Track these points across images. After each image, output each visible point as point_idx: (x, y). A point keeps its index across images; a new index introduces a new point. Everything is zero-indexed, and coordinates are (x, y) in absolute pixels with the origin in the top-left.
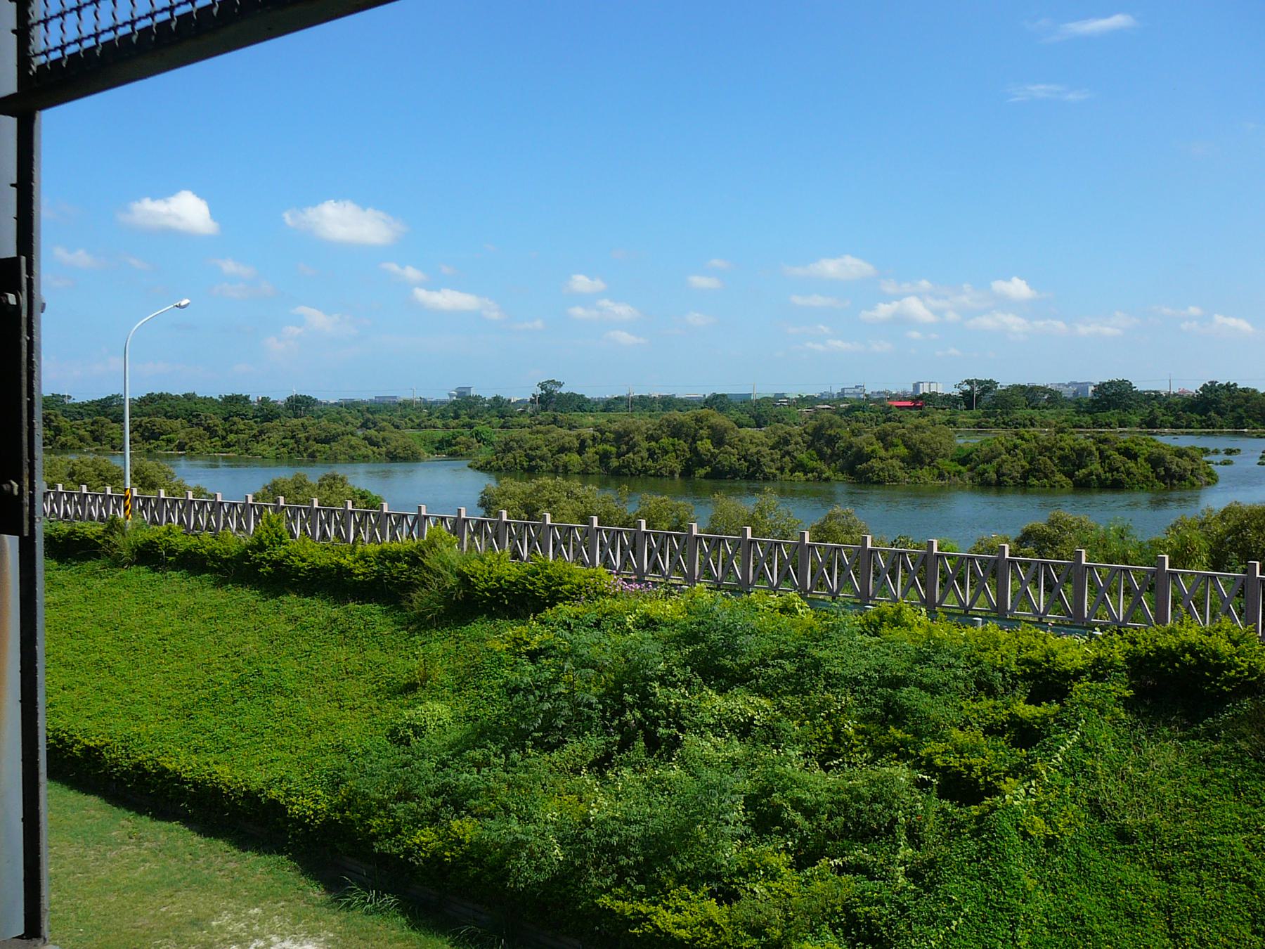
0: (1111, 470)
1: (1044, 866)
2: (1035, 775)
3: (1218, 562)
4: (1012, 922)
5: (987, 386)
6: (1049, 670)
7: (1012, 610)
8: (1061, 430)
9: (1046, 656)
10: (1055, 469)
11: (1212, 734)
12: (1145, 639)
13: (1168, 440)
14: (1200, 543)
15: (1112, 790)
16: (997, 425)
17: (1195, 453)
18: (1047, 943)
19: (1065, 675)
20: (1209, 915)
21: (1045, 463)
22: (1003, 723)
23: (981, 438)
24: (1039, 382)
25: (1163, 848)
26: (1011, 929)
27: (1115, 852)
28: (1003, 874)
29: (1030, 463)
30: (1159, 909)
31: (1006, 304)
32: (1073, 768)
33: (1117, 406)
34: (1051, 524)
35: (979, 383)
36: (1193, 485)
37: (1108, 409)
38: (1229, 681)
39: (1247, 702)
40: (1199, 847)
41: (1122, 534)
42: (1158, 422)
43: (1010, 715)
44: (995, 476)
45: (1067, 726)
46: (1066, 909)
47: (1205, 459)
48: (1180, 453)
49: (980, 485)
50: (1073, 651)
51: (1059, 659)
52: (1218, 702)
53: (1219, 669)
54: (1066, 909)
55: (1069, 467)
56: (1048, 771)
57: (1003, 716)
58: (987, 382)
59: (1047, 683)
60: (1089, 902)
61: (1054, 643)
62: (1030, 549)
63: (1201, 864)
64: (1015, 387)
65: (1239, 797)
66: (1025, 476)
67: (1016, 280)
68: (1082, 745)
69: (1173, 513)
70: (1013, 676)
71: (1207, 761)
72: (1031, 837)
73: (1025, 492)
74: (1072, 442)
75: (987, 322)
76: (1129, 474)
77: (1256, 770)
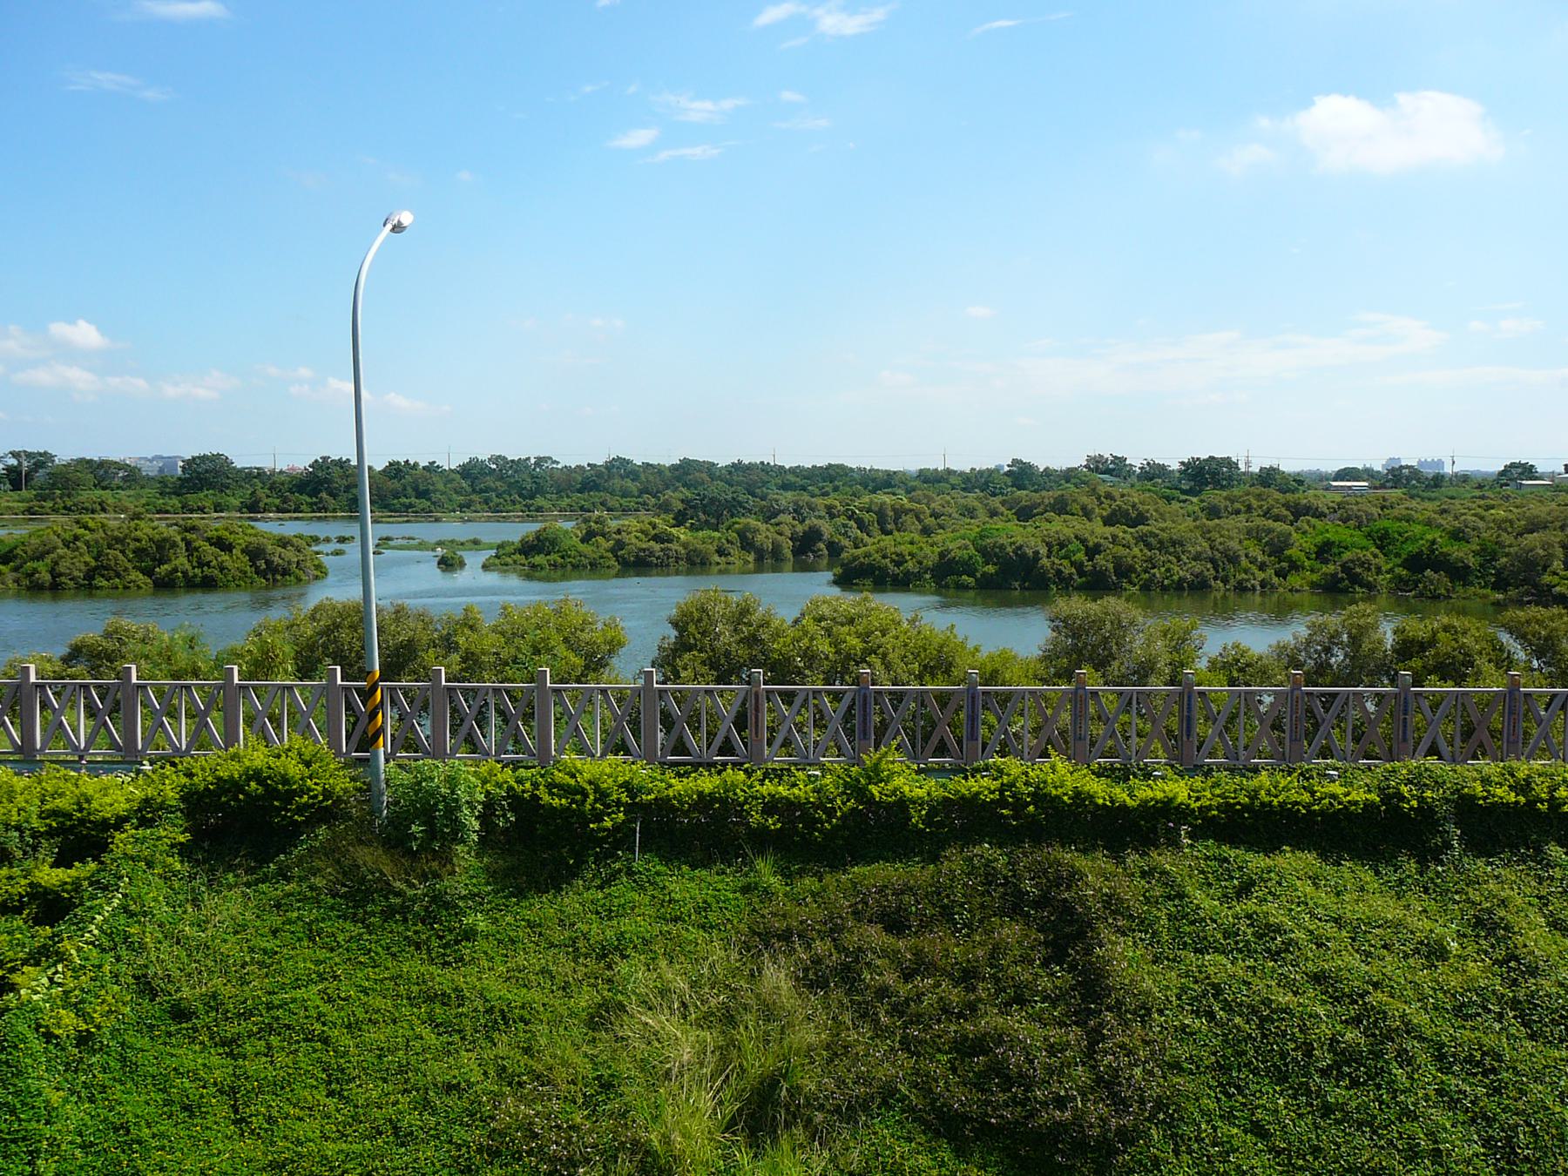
0: (201, 565)
1: (76, 1072)
2: (62, 957)
3: (306, 669)
4: (30, 1153)
5: (41, 460)
6: (82, 821)
7: (43, 748)
8: (137, 516)
9: (79, 804)
10: (129, 565)
11: (284, 874)
12: (203, 769)
13: (272, 527)
14: (285, 650)
15: (163, 959)
16: (55, 510)
17: (302, 543)
18: (81, 1168)
19: (104, 825)
20: (278, 1087)
21: (116, 559)
22: (22, 896)
23: (33, 527)
24: (115, 457)
25: (227, 1019)
26: (29, 1163)
27: (169, 1034)
28: (17, 1094)
29: (96, 559)
30: (222, 1093)
31: (70, 353)
32: (114, 941)
33: (211, 486)
34: (108, 635)
35: (29, 455)
36: (299, 580)
37: (201, 489)
38: (300, 810)
39: (322, 831)
40: (269, 1009)
41: (191, 643)
42: (261, 505)
43: (31, 885)
44: (48, 577)
45: (105, 888)
46: (106, 1119)
47: (315, 548)
48: (284, 543)
49: (28, 588)
50: (114, 793)
51: (95, 805)
52: (291, 834)
53: (290, 795)
54: (106, 1119)
55: (148, 563)
56: (79, 950)
57: (21, 886)
58: (40, 454)
59: (80, 837)
60: (135, 1103)
61: (89, 785)
62: (79, 668)
63: (272, 1029)
64: (82, 461)
65: (314, 942)
66: (90, 575)
67: (82, 324)
68: (125, 909)
69: (277, 614)
70: (35, 834)
71: (278, 906)
72: (57, 1037)
73: (91, 596)
74: (150, 532)
75: (42, 376)
76: (222, 569)
77: (332, 908)
